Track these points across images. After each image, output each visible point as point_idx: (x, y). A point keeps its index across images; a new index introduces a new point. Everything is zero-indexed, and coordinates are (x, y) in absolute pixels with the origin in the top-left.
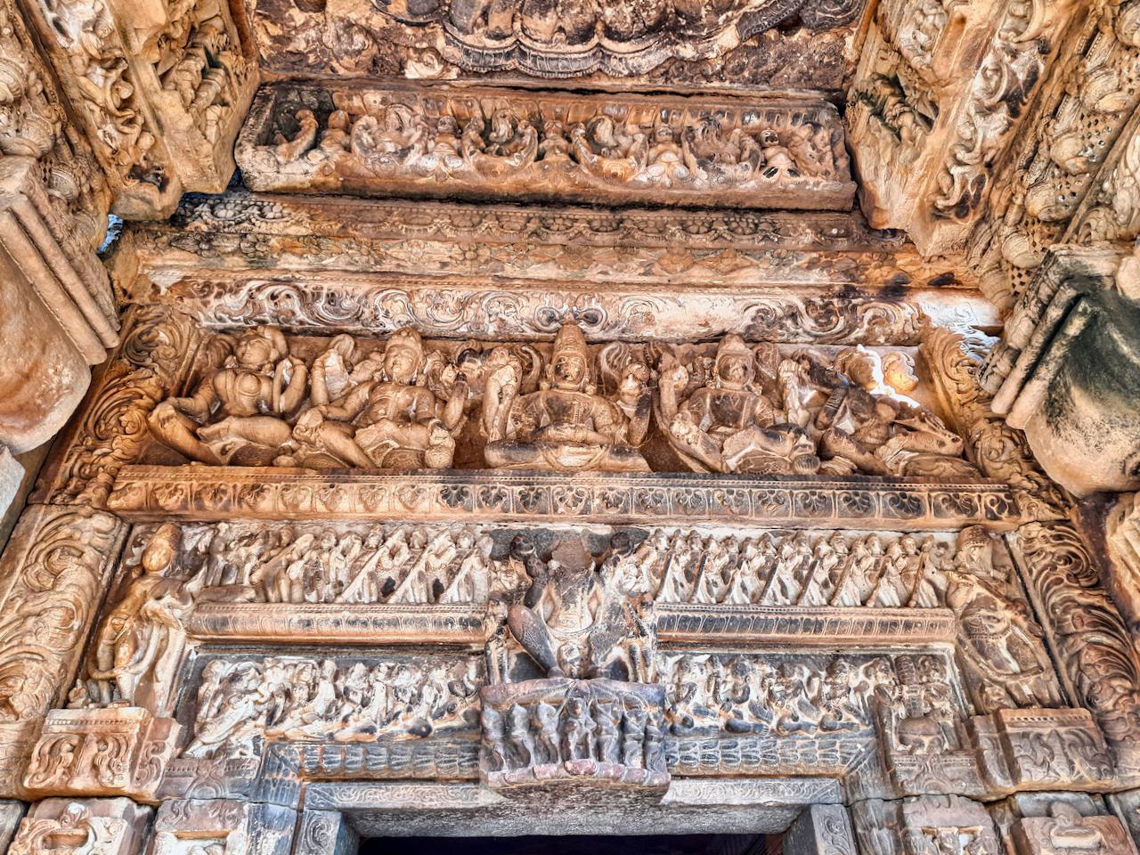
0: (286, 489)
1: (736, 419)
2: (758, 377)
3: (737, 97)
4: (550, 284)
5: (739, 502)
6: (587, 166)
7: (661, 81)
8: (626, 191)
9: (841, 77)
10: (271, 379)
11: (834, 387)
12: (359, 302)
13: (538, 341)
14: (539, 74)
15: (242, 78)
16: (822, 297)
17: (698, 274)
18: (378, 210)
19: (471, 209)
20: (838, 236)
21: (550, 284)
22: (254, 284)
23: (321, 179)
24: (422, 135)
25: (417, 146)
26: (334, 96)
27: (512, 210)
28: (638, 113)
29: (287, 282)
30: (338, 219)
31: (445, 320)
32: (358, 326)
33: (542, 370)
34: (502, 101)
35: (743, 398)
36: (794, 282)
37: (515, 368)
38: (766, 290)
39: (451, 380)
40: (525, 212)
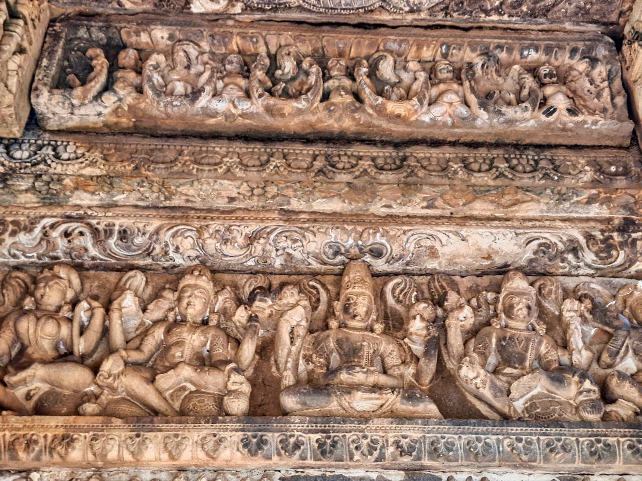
0: (95, 438)
1: (522, 360)
2: (542, 314)
3: (516, 30)
4: (335, 218)
5: (527, 450)
6: (372, 107)
7: (441, 16)
8: (409, 130)
9: (617, 11)
10: (70, 320)
11: (617, 328)
12: (150, 238)
13: (324, 274)
14: (322, 10)
15: (37, 20)
16: (602, 231)
17: (480, 208)
18: (170, 149)
19: (258, 147)
20: (616, 174)
21: (335, 218)
22: (47, 222)
23: (114, 120)
24: (211, 77)
25: (208, 88)
26: (123, 32)
27: (298, 147)
28: (419, 48)
29: (80, 219)
30: (131, 159)
31: (234, 253)
32: (149, 261)
33: (330, 305)
34: (287, 37)
35: (528, 340)
36: (575, 215)
37: (305, 307)
38: (547, 223)
39: (244, 320)
40: (311, 149)
